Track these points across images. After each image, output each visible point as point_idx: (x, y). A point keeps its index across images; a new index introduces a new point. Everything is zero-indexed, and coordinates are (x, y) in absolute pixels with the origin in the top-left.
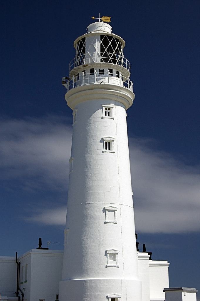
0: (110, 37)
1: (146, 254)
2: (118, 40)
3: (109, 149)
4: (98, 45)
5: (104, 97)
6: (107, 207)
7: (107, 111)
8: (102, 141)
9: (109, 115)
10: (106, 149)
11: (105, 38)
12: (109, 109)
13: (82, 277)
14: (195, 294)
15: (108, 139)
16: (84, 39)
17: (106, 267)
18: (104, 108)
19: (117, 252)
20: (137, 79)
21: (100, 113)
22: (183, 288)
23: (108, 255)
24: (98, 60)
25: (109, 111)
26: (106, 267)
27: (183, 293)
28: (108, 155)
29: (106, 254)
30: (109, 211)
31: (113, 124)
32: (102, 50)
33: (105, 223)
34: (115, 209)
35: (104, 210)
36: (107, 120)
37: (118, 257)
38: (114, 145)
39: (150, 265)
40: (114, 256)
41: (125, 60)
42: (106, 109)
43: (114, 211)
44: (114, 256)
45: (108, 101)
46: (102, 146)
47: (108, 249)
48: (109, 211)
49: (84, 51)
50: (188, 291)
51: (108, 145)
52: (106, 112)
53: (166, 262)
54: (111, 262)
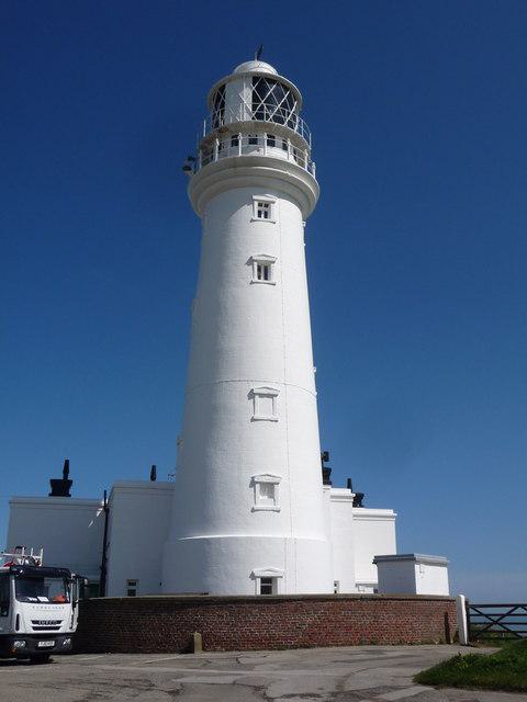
0: (271, 80)
1: (347, 492)
2: (286, 89)
3: (266, 278)
4: (247, 95)
5: (257, 181)
6: (257, 388)
7: (263, 209)
8: (251, 261)
9: (266, 217)
10: (259, 278)
11: (261, 82)
12: (267, 206)
13: (216, 533)
14: (444, 570)
15: (261, 258)
16: (222, 89)
17: (253, 510)
18: (256, 203)
19: (275, 480)
20: (325, 159)
21: (249, 211)
22: (417, 556)
23: (258, 486)
24: (246, 116)
25: (266, 209)
26: (253, 510)
27: (417, 567)
28: (263, 288)
29: (253, 483)
30: (261, 395)
31: (278, 234)
32: (255, 99)
33: (253, 420)
34: (275, 393)
35: (252, 395)
36: (262, 224)
37: (279, 490)
38: (275, 270)
39: (354, 516)
40: (269, 488)
41: (305, 128)
42: (260, 205)
43: (272, 396)
44: (269, 488)
45: (263, 189)
46: (251, 273)
47: (259, 474)
48: (261, 395)
49: (223, 105)
50: (427, 563)
51: (264, 271)
52: (260, 213)
53: (390, 512)
54: (263, 501)
